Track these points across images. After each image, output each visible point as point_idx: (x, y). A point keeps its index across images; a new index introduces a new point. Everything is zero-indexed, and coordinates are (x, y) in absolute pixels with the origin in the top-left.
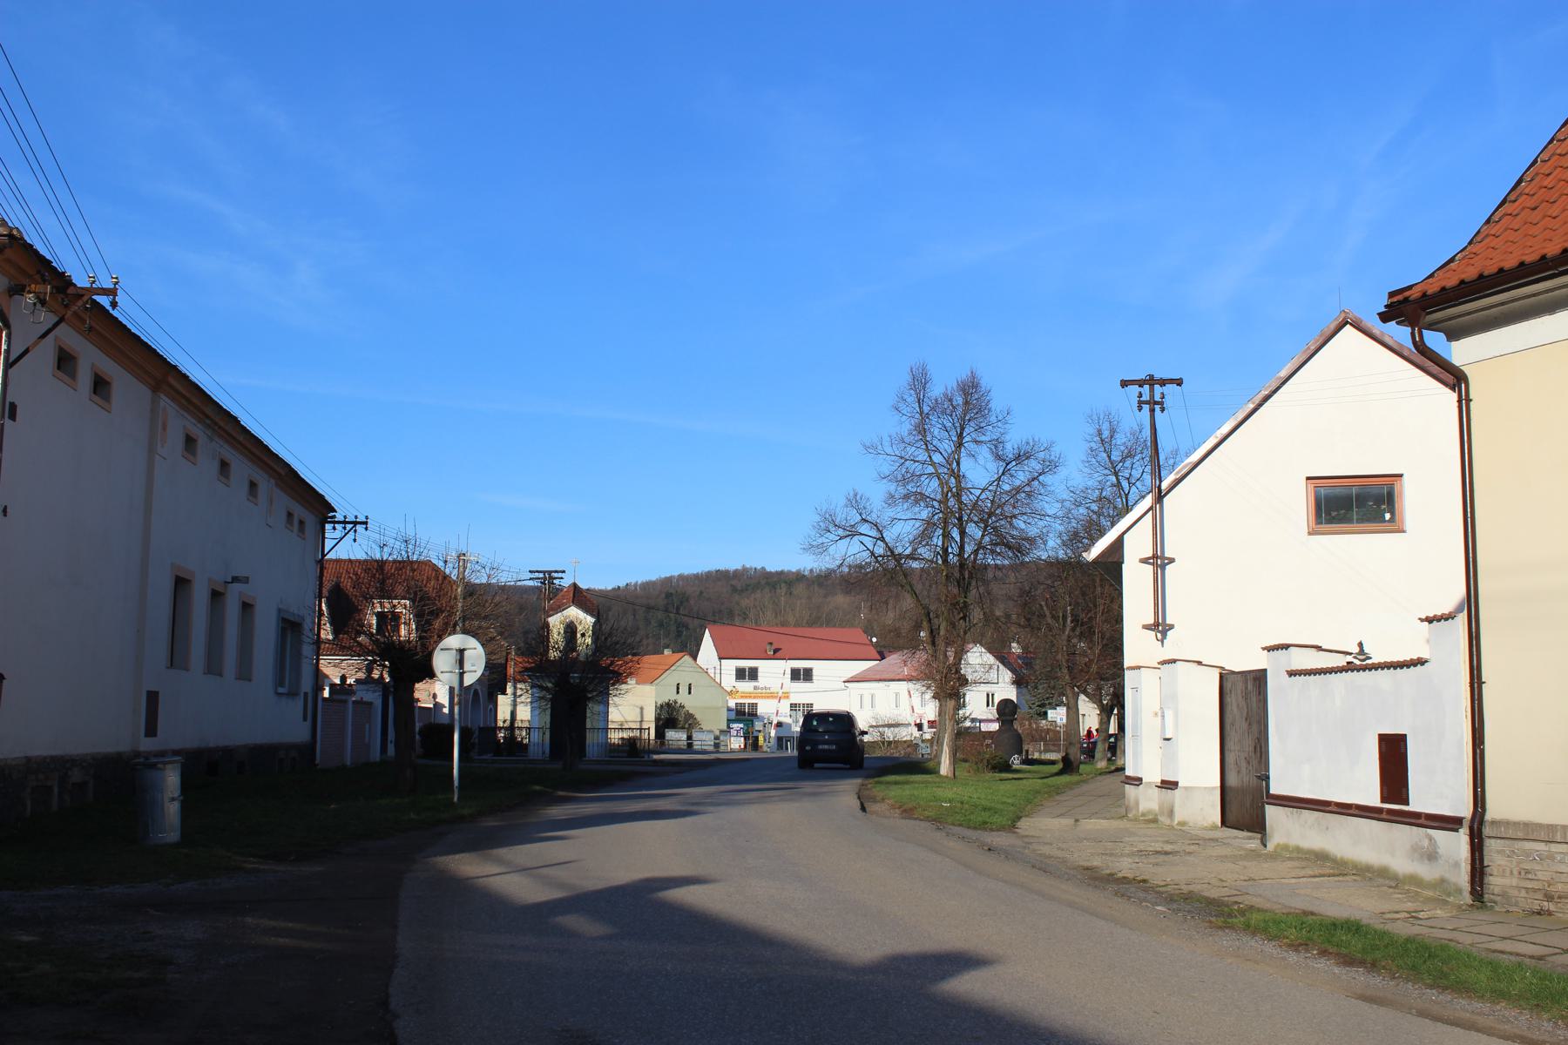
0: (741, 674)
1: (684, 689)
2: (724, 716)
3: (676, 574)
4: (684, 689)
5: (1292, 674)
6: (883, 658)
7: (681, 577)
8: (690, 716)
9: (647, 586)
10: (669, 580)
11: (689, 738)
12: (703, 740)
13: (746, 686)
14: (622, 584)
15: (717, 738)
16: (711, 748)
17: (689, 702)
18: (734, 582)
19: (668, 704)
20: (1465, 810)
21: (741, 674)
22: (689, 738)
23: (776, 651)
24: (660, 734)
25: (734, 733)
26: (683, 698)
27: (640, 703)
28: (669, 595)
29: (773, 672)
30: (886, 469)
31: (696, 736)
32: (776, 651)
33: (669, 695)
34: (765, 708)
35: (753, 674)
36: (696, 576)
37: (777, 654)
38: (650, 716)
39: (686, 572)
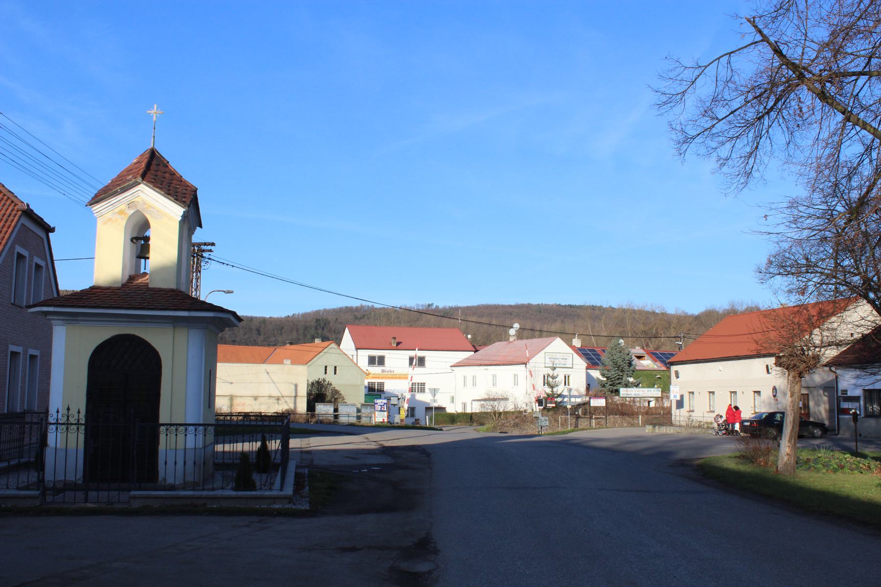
0: (372, 361)
1: (330, 370)
2: (363, 392)
3: (322, 308)
4: (330, 370)
5: (326, 367)
6: (476, 351)
7: (325, 310)
8: (336, 392)
9: (305, 315)
10: (318, 312)
11: (336, 410)
12: (347, 414)
13: (376, 370)
14: (291, 314)
15: (359, 411)
16: (332, 419)
17: (335, 381)
18: (356, 314)
19: (318, 382)
20: (294, 394)
21: (372, 361)
22: (336, 410)
23: (398, 344)
24: (311, 407)
25: (378, 408)
26: (330, 378)
27: (294, 382)
28: (317, 320)
29: (397, 360)
30: (735, 171)
31: (342, 410)
32: (398, 344)
33: (319, 375)
34: (390, 386)
35: (381, 361)
36: (334, 310)
37: (399, 346)
38: (303, 391)
39: (328, 308)
